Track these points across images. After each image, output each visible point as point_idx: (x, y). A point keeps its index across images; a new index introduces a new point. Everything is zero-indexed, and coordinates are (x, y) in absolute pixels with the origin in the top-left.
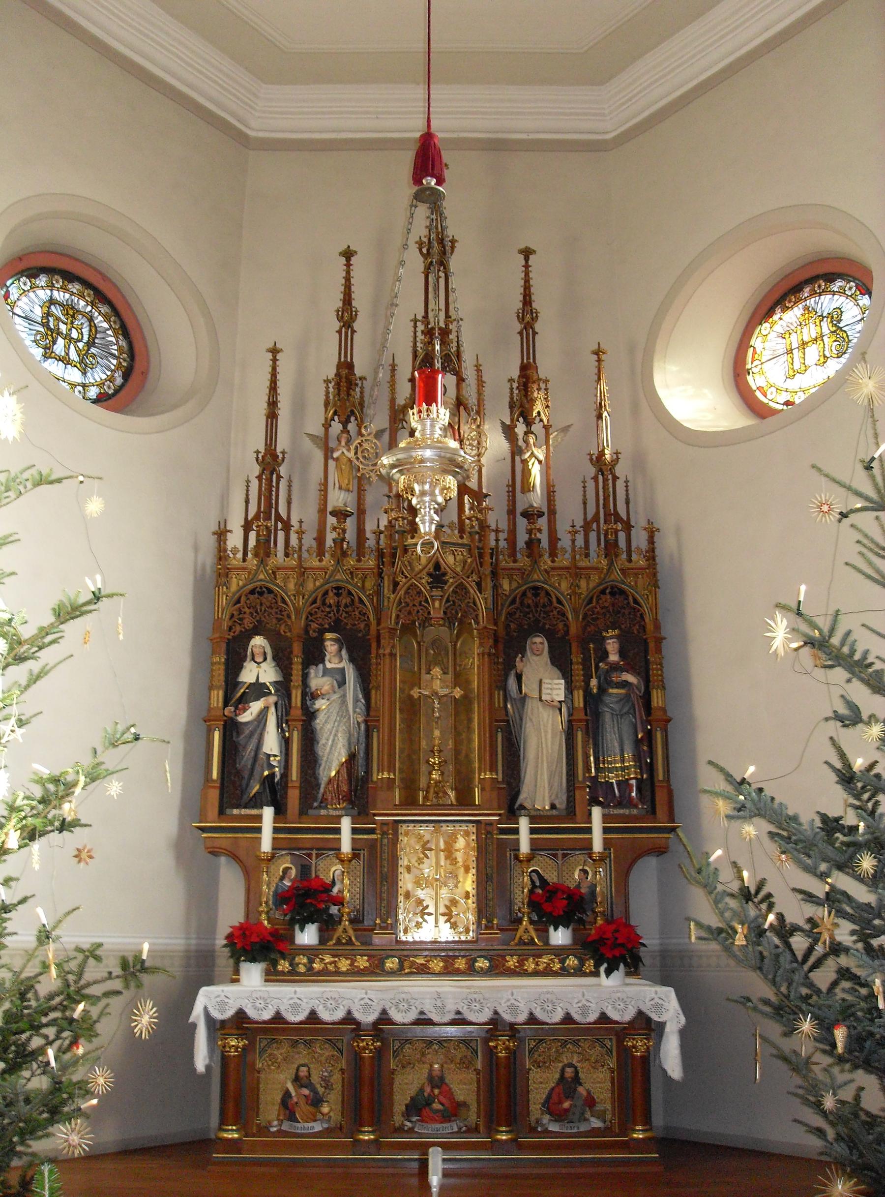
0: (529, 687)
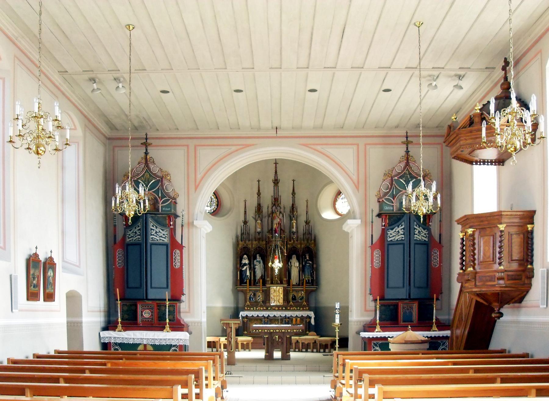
0: (293, 264)
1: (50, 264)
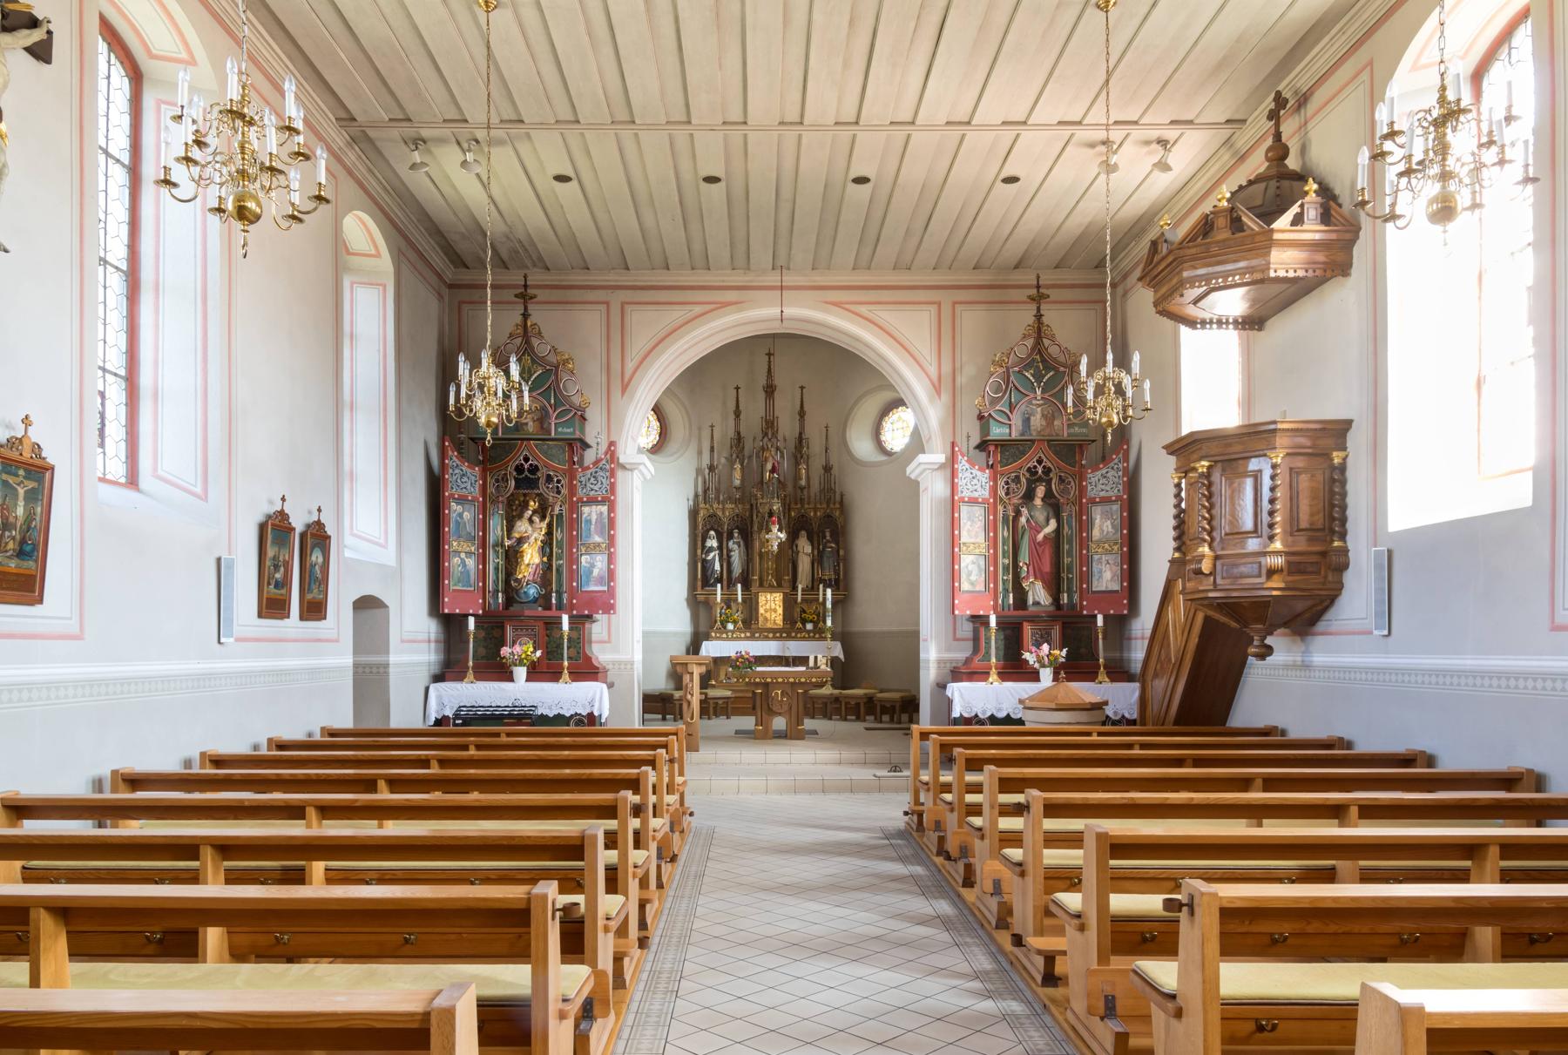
1: (317, 537)
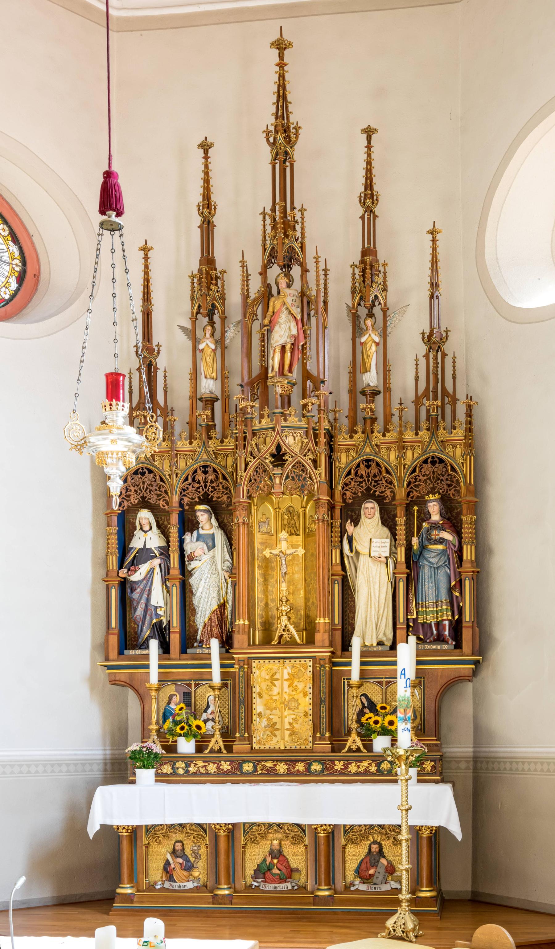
0: (361, 545)
